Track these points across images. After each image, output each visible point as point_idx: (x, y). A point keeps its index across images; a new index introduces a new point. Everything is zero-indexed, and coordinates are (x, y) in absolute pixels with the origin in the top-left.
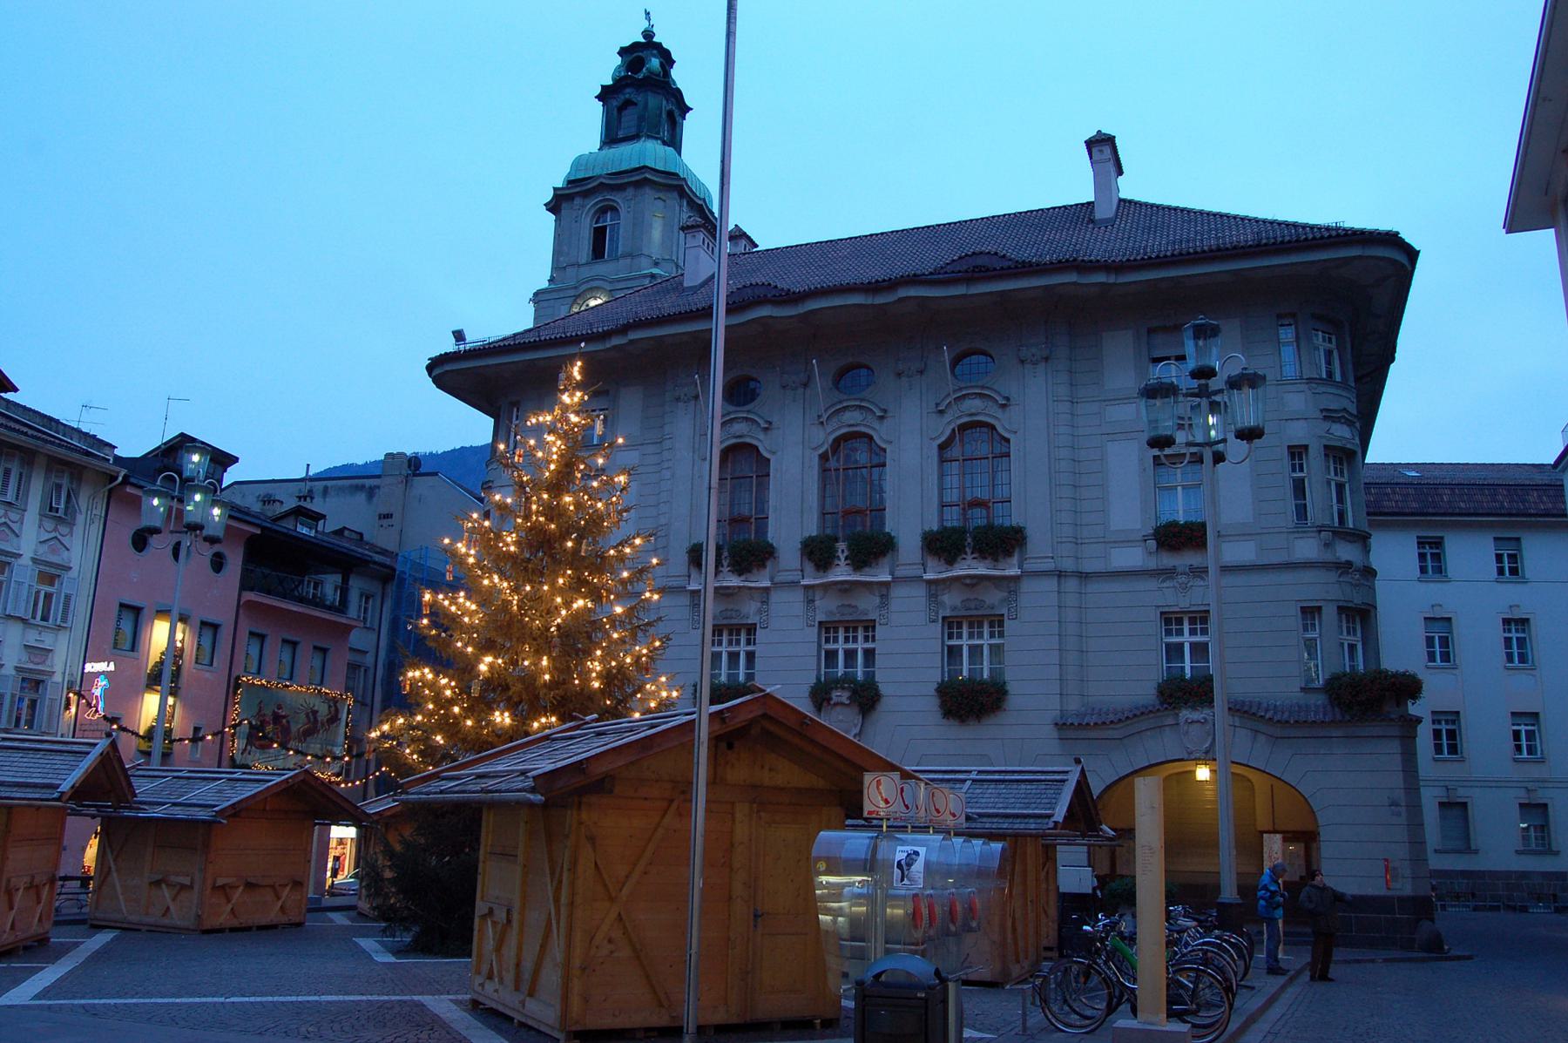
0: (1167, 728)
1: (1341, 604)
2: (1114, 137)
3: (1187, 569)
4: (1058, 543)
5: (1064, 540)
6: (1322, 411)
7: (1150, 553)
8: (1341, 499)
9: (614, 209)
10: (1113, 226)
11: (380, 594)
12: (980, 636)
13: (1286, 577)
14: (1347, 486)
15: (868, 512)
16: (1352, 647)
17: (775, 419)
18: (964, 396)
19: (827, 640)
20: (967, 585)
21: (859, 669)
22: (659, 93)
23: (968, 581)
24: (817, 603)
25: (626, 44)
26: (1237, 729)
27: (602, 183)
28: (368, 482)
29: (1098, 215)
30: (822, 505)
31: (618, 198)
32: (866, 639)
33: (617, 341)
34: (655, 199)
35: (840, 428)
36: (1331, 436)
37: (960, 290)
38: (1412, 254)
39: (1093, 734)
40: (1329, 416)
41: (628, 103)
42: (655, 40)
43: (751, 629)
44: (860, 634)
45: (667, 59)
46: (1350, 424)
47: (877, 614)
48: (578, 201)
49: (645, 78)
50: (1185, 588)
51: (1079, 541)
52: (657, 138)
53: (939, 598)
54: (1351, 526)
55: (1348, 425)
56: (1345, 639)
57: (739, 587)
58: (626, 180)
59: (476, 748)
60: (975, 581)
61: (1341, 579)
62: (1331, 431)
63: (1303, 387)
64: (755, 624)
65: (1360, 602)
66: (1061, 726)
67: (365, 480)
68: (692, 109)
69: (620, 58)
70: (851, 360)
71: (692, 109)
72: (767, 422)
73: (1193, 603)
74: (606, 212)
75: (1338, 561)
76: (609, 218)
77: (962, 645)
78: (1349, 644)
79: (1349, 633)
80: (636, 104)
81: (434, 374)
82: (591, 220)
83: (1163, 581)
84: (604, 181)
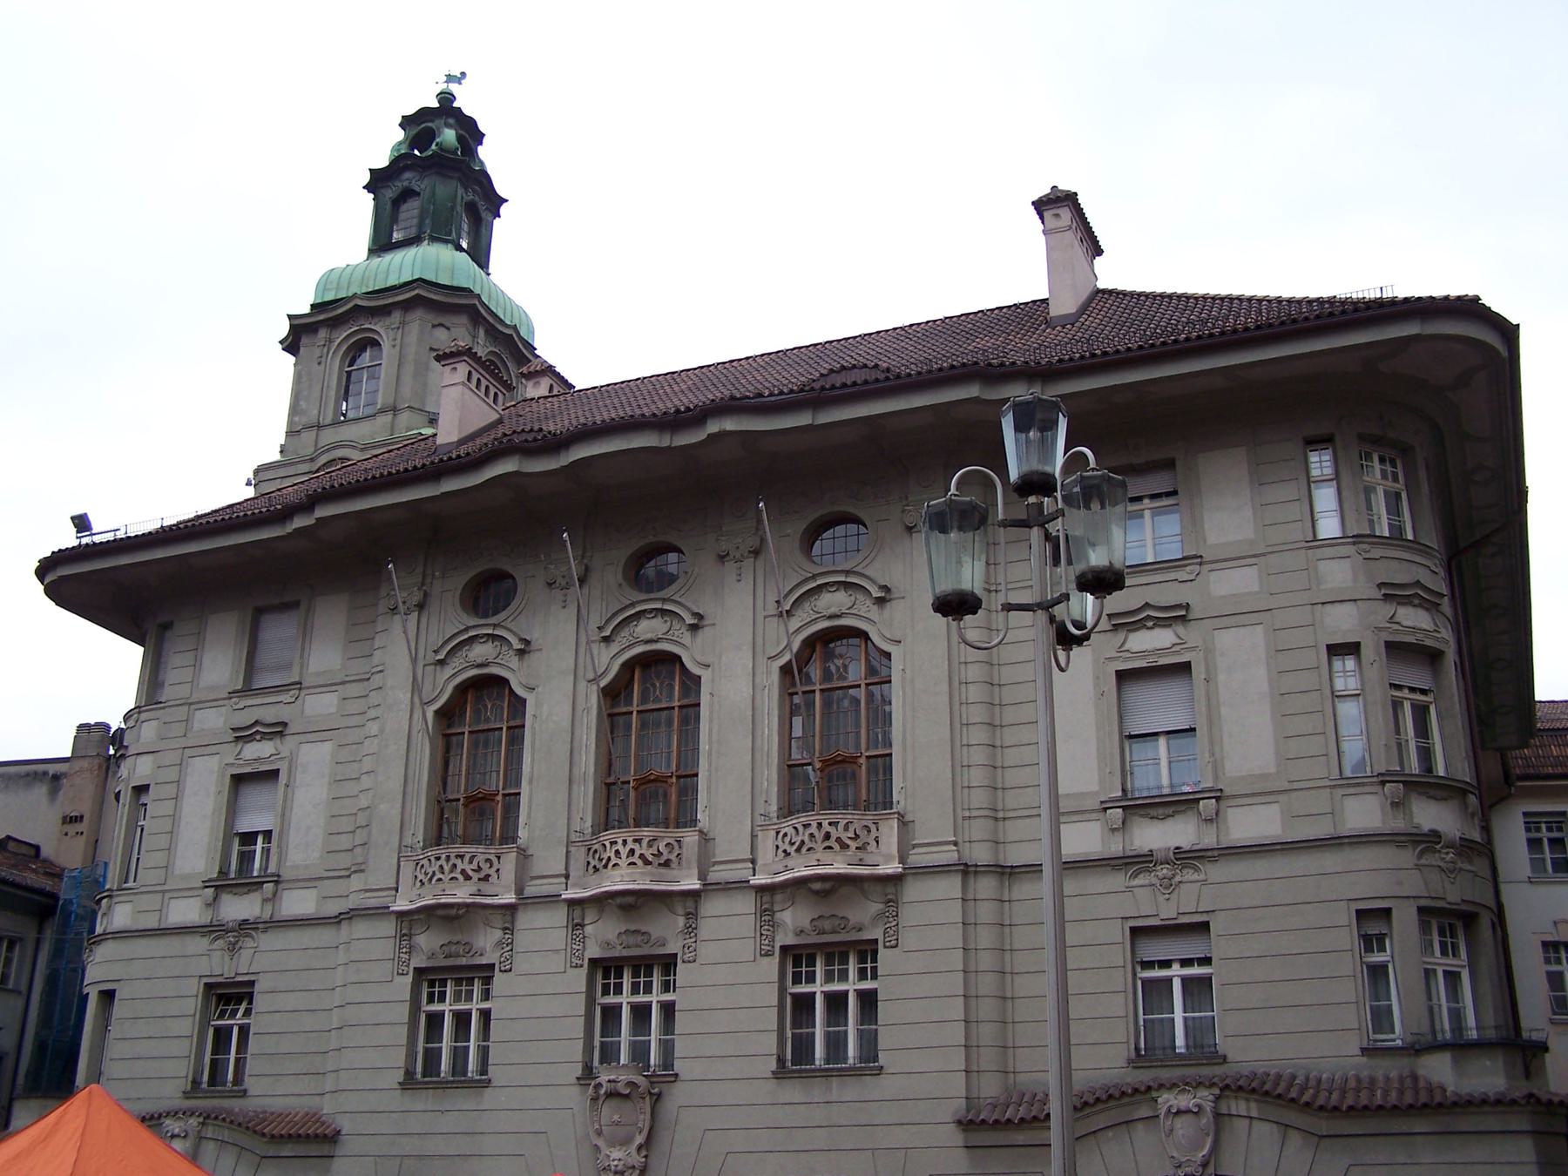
0: (1140, 1126)
1: (1423, 903)
2: (1076, 194)
3: (1171, 854)
4: (964, 818)
5: (974, 813)
6: (1381, 585)
7: (1113, 830)
8: (1422, 730)
9: (375, 344)
10: (1073, 325)
11: (33, 935)
12: (844, 976)
13: (1330, 861)
14: (1432, 709)
15: (674, 780)
16: (1452, 977)
17: (535, 635)
18: (820, 588)
19: (606, 992)
20: (817, 893)
21: (653, 1037)
22: (451, 178)
23: (817, 886)
24: (589, 929)
25: (411, 111)
26: (1255, 1123)
27: (356, 305)
28: (52, 769)
29: (1055, 311)
30: (607, 763)
31: (381, 328)
32: (862, 975)
33: (299, 522)
34: (434, 326)
35: (630, 647)
36: (1396, 627)
37: (803, 419)
38: (1509, 333)
39: (1020, 1138)
40: (1392, 594)
41: (408, 194)
42: (455, 105)
43: (486, 973)
44: (852, 968)
45: (471, 133)
46: (1431, 606)
47: (680, 944)
48: (323, 333)
49: (435, 155)
50: (1169, 885)
51: (1001, 815)
52: (446, 242)
53: (778, 915)
54: (1441, 773)
55: (1427, 609)
56: (1439, 964)
57: (467, 905)
58: (391, 300)
59: (872, 1059)
60: (828, 886)
61: (1423, 861)
62: (1396, 619)
63: (1350, 550)
64: (675, 955)
65: (1459, 901)
66: (967, 1124)
67: (49, 765)
68: (507, 201)
69: (403, 132)
70: (651, 539)
71: (507, 201)
72: (523, 640)
73: (1180, 912)
74: (364, 350)
75: (1414, 831)
76: (368, 358)
77: (815, 993)
78: (1445, 972)
79: (1444, 953)
80: (418, 194)
81: (45, 583)
82: (343, 360)
83: (1135, 875)
84: (360, 303)
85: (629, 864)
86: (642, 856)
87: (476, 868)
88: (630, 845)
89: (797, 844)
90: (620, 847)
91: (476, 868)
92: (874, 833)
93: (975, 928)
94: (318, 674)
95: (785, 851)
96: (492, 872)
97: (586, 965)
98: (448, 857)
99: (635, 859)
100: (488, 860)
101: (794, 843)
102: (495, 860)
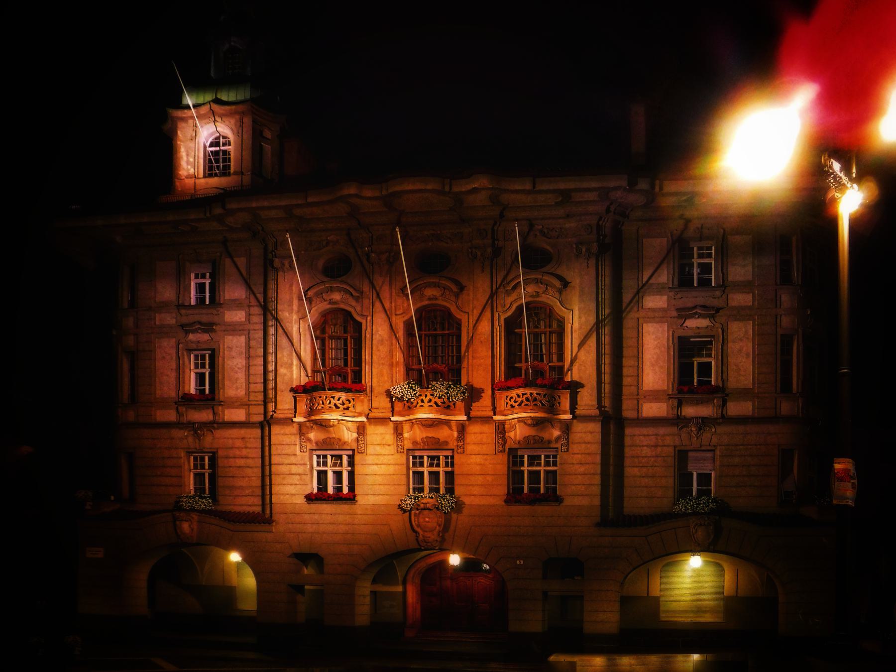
21: (441, 485)
85: (534, 405)
87: (342, 403)
89: (519, 402)
90: (423, 398)
91: (342, 403)
97: (405, 452)
99: (432, 403)
101: (517, 402)
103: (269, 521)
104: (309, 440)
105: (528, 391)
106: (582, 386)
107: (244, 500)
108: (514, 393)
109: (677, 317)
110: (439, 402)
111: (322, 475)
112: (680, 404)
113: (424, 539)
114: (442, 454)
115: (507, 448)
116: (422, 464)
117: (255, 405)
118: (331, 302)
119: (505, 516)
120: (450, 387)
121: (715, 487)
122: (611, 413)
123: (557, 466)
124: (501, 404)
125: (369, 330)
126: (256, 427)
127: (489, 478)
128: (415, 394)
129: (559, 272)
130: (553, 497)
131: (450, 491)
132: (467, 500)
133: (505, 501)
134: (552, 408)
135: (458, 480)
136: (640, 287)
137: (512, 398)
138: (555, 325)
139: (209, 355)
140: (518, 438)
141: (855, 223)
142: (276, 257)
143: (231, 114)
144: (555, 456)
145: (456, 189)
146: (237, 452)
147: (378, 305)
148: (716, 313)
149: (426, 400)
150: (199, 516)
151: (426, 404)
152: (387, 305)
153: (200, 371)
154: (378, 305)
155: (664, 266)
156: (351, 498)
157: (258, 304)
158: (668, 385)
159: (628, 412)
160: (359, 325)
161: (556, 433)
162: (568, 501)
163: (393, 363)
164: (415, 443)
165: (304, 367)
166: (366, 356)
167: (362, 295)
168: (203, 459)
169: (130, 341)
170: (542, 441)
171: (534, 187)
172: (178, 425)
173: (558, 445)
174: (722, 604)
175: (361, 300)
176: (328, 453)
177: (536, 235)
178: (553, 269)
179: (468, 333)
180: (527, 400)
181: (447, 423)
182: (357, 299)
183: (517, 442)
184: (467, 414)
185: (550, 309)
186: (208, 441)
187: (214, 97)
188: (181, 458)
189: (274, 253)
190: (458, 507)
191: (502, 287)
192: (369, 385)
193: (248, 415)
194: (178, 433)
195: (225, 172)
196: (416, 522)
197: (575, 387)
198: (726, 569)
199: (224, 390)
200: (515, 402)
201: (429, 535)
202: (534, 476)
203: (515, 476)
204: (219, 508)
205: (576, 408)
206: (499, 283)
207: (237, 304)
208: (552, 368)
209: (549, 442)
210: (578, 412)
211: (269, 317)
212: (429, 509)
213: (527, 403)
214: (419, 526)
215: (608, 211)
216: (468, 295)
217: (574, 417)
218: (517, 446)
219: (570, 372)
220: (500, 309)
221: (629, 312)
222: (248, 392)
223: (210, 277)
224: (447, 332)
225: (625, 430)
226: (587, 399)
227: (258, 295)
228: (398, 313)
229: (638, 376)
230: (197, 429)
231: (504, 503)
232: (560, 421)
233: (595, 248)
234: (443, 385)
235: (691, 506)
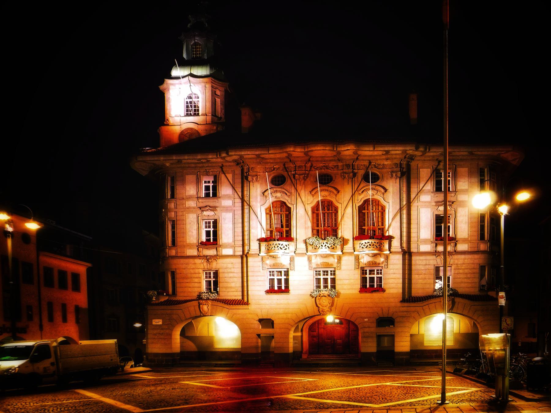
86: (328, 247)
88: (325, 244)
90: (322, 244)
92: (288, 246)
93: (204, 267)
94: (221, 175)
95: (315, 248)
96: (287, 248)
98: (276, 244)
99: (326, 247)
100: (286, 245)
102: (288, 245)
103: (247, 303)
104: (266, 264)
105: (370, 241)
106: (393, 238)
107: (231, 294)
108: (363, 242)
109: (435, 206)
110: (329, 246)
111: (272, 281)
112: (436, 245)
113: (322, 311)
114: (329, 270)
115: (360, 267)
116: (320, 275)
117: (238, 247)
118: (276, 197)
119: (237, 273)
120: (335, 239)
121: (452, 283)
122: (406, 250)
123: (382, 275)
124: (357, 246)
125: (295, 211)
126: (238, 258)
127: (352, 281)
128: (319, 243)
129: (382, 185)
130: (380, 289)
131: (334, 287)
132: (342, 292)
133: (360, 292)
134: (381, 249)
135: (337, 282)
136: (418, 191)
137: (362, 244)
138: (380, 208)
139: (213, 222)
140: (365, 262)
141: (506, 217)
142: (249, 176)
143: (200, 83)
144: (381, 270)
145: (339, 149)
146: (229, 270)
147: (299, 199)
148: (452, 204)
149: (324, 245)
150: (212, 302)
151: (324, 247)
152: (303, 199)
153: (208, 229)
154: (299, 199)
155: (430, 181)
156: (287, 290)
157: (239, 197)
158: (431, 236)
159: (413, 249)
160: (290, 208)
161: (382, 259)
162: (387, 291)
163: (306, 227)
164: (317, 265)
165: (263, 229)
166: (293, 223)
167: (291, 194)
168: (210, 273)
169: (173, 215)
170: (376, 263)
171: (374, 149)
172: (198, 257)
173: (383, 265)
174: (453, 337)
175: (290, 197)
176: (275, 270)
177: (372, 167)
178: (380, 183)
179: (341, 213)
180: (370, 245)
181: (332, 255)
182: (289, 196)
183: (364, 264)
184: (342, 251)
185: (378, 202)
186: (215, 265)
187: (190, 73)
188: (200, 273)
189: (247, 173)
190: (338, 295)
191: (357, 191)
192: (295, 237)
193: (234, 251)
194: (198, 261)
195: (196, 114)
196: (319, 302)
197: (390, 238)
198: (455, 320)
199: (222, 240)
200: (364, 246)
201: (325, 308)
202: (372, 279)
203: (364, 280)
204: (220, 298)
205: (391, 248)
206: (355, 189)
207: (228, 197)
208: (379, 229)
209: (379, 264)
210: (392, 250)
211: (245, 204)
212: (325, 296)
213: (370, 246)
214: (320, 304)
215: (405, 157)
216: (341, 195)
217: (391, 253)
218: (365, 266)
219: (388, 231)
220: (356, 201)
221: (414, 203)
222: (234, 241)
223: (212, 183)
224: (331, 212)
225: (412, 257)
226: (396, 243)
227: (238, 193)
228: (309, 203)
229: (418, 232)
230: (208, 259)
231: (359, 293)
232: (384, 254)
233: (399, 174)
234: (332, 238)
235: (442, 292)
